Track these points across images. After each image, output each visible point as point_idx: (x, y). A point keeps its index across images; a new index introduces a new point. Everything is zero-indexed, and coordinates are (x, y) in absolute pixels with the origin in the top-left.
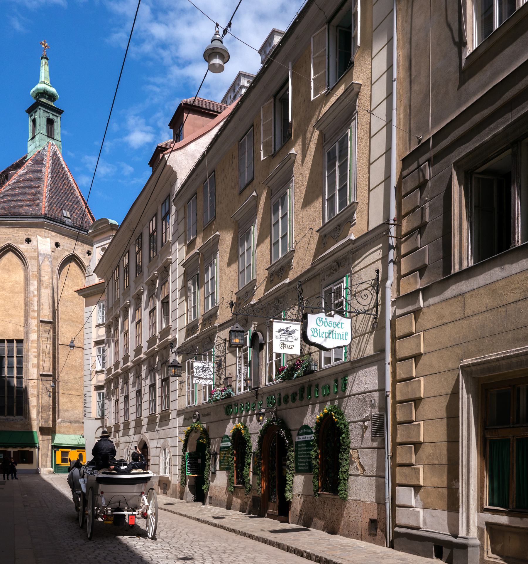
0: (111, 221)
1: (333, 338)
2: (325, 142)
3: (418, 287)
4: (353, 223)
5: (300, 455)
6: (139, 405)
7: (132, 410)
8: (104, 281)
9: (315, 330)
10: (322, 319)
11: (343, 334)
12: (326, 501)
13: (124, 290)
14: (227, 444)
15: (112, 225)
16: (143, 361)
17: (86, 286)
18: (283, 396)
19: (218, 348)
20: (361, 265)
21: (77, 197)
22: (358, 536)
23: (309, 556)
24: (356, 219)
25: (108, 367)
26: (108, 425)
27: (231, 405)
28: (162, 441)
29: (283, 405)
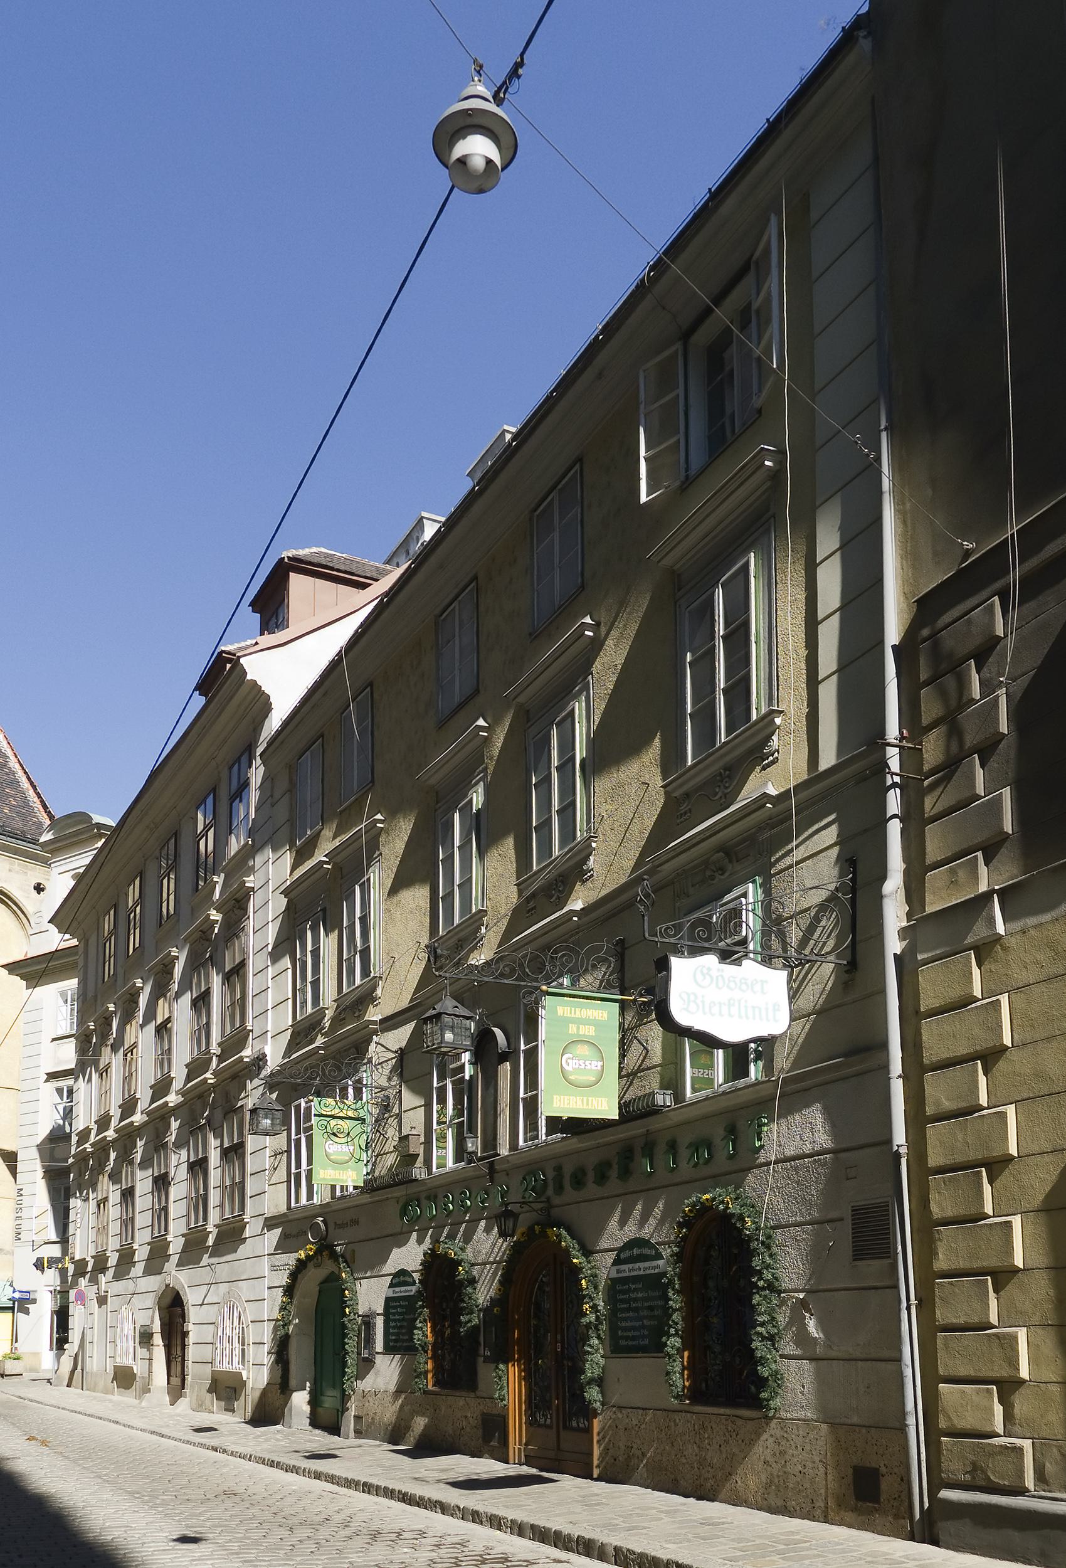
0: (97, 819)
1: (740, 1017)
2: (679, 590)
3: (983, 887)
4: (771, 758)
5: (623, 1310)
6: (161, 1209)
7: (143, 1219)
8: (77, 943)
9: (692, 998)
10: (709, 969)
11: (767, 1009)
12: (706, 1424)
13: (161, 925)
14: (406, 1291)
15: (99, 826)
16: (139, 1128)
17: (29, 956)
18: (568, 1171)
19: (380, 1070)
20: (797, 855)
21: (14, 773)
22: (818, 1512)
23: (587, 1548)
24: (778, 751)
25: (81, 1128)
26: (77, 1258)
27: (436, 1197)
28: (223, 1288)
29: (570, 1194)
